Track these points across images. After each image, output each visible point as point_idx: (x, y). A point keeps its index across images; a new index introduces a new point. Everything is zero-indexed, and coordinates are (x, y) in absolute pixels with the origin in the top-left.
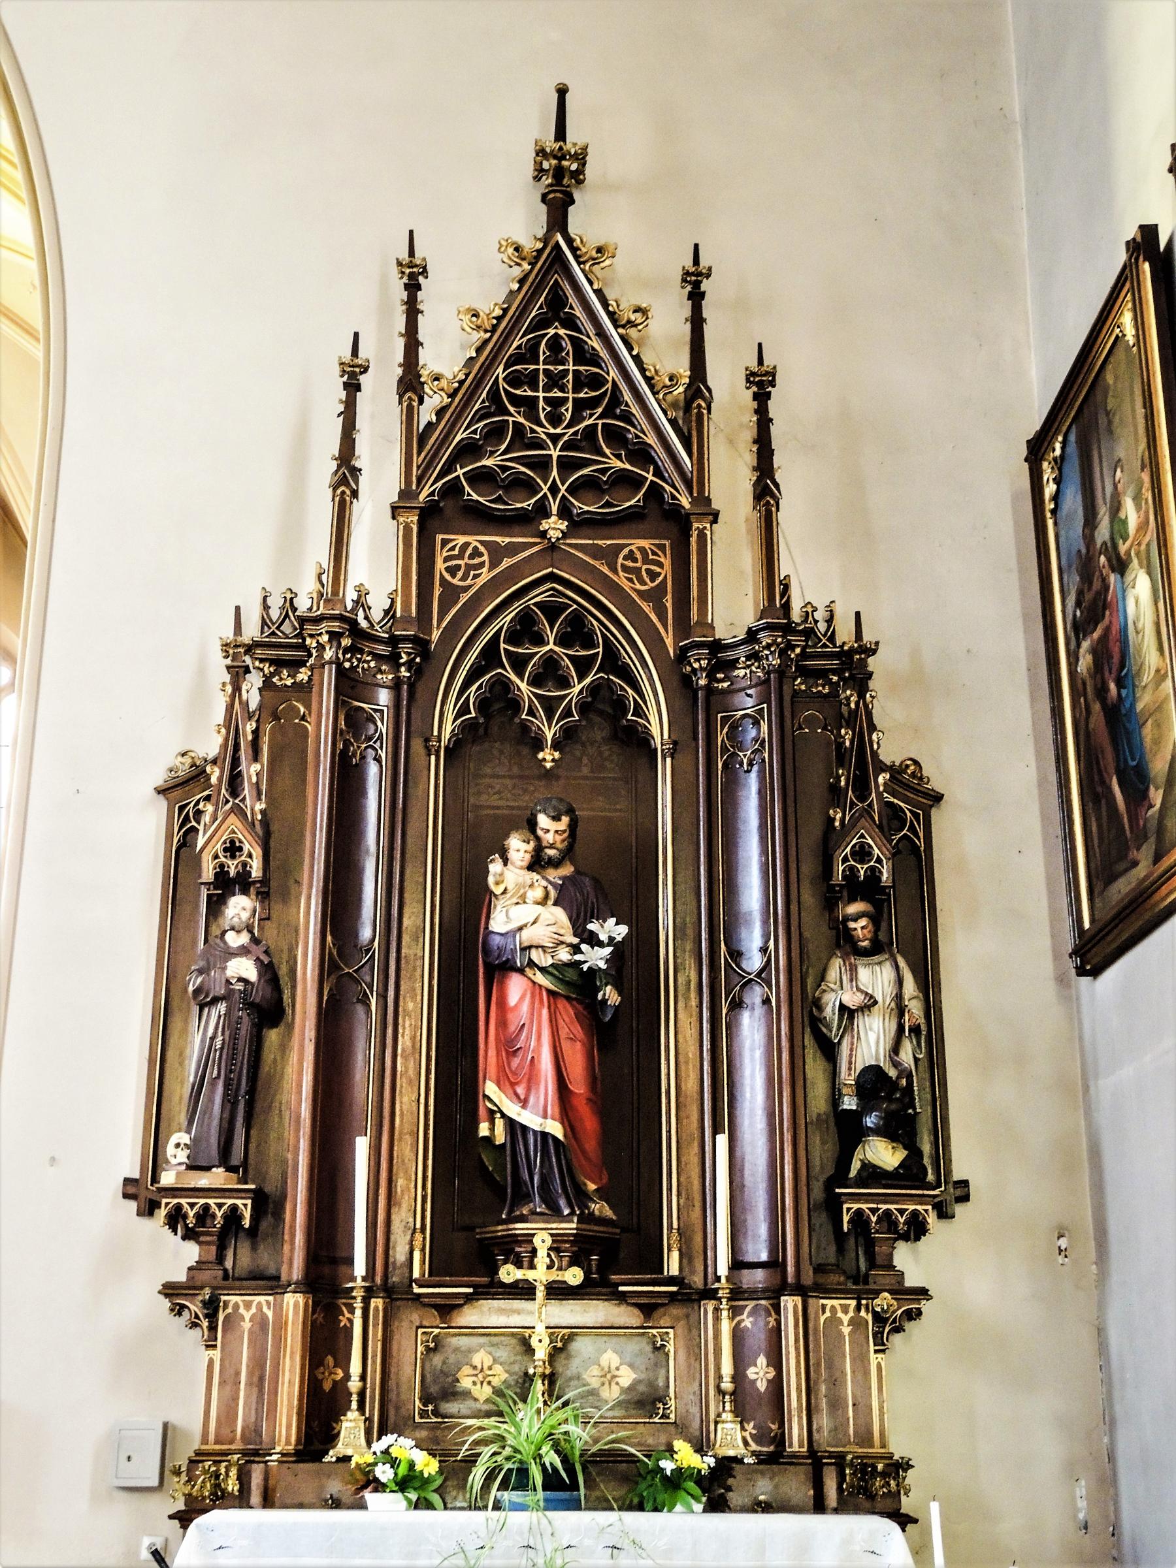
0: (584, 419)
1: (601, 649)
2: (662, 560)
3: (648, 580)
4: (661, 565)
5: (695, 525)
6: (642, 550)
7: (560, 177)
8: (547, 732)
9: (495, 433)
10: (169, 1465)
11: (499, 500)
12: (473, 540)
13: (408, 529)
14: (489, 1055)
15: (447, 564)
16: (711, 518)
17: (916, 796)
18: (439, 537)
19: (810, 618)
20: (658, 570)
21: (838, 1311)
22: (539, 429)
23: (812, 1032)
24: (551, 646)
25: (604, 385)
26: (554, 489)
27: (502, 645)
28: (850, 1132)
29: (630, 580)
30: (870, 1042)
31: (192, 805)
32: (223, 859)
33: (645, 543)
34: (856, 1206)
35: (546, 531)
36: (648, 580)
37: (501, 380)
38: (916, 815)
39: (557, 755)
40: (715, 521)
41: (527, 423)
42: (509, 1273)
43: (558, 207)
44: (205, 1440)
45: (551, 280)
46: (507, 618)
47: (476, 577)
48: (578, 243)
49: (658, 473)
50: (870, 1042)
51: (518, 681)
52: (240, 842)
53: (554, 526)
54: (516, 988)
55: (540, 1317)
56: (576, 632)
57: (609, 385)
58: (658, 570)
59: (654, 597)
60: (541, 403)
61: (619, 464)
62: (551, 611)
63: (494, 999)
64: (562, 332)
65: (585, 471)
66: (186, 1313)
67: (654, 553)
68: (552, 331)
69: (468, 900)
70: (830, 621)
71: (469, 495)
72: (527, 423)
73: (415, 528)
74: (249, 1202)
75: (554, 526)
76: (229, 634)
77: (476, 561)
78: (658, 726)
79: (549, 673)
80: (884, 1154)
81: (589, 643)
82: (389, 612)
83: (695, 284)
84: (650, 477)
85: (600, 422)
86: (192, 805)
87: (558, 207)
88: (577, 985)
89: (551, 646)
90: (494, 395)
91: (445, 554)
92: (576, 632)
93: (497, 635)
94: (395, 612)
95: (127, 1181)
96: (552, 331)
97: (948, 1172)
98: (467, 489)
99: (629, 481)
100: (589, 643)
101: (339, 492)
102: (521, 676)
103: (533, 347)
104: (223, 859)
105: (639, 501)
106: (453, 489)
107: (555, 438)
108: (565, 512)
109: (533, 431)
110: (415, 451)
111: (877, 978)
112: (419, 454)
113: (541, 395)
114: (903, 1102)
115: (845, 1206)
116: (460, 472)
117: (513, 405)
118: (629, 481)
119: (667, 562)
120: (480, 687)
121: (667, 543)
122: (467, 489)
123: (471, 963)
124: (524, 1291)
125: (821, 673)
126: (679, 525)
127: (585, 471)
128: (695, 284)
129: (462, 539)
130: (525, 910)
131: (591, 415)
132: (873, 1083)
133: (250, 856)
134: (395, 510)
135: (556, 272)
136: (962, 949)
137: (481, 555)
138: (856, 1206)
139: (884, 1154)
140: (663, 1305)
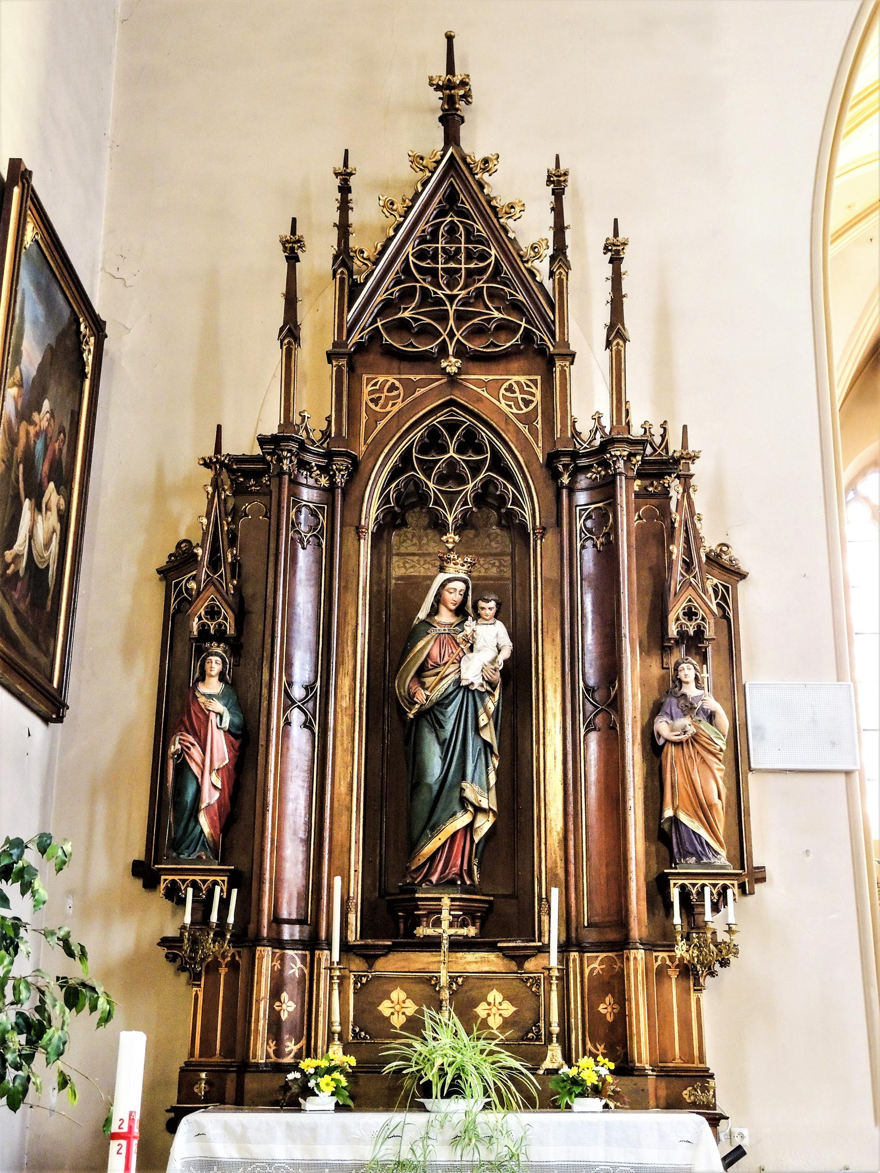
0: (474, 282)
1: (489, 455)
2: (534, 390)
3: (523, 407)
4: (533, 395)
5: (558, 364)
6: (518, 383)
8: (448, 516)
9: (407, 295)
11: (411, 345)
12: (391, 379)
13: (339, 368)
15: (371, 397)
16: (570, 358)
18: (365, 377)
19: (648, 434)
20: (530, 398)
22: (439, 292)
24: (451, 453)
25: (488, 259)
26: (451, 335)
27: (414, 454)
29: (510, 406)
31: (184, 582)
32: (205, 621)
33: (522, 379)
34: (170, 878)
35: (445, 368)
36: (523, 407)
37: (411, 258)
38: (727, 588)
39: (457, 538)
40: (572, 363)
41: (431, 288)
42: (423, 931)
43: (451, 121)
44: (192, 1054)
46: (417, 434)
47: (393, 405)
48: (469, 160)
49: (528, 322)
51: (428, 482)
52: (218, 607)
53: (452, 365)
55: (444, 966)
56: (470, 443)
57: (493, 258)
58: (530, 398)
59: (527, 420)
60: (440, 272)
61: (501, 316)
62: (452, 427)
64: (456, 219)
65: (476, 321)
66: (179, 960)
67: (528, 386)
68: (449, 219)
70: (663, 436)
71: (386, 340)
72: (431, 288)
73: (345, 369)
74: (226, 879)
75: (452, 365)
76: (210, 452)
77: (395, 393)
81: (480, 450)
82: (326, 434)
83: (557, 183)
84: (523, 324)
85: (485, 285)
86: (184, 582)
87: (451, 121)
89: (451, 453)
90: (406, 270)
91: (369, 388)
93: (410, 448)
94: (330, 433)
95: (763, 880)
96: (449, 219)
98: (385, 336)
99: (506, 328)
100: (480, 450)
101: (286, 341)
102: (429, 477)
103: (434, 234)
104: (205, 621)
105: (517, 341)
106: (375, 335)
107: (451, 298)
108: (461, 352)
109: (435, 293)
110: (346, 305)
112: (349, 311)
113: (440, 266)
115: (163, 877)
116: (379, 324)
117: (419, 273)
118: (506, 328)
119: (538, 393)
120: (397, 485)
121: (539, 378)
122: (385, 336)
124: (432, 944)
126: (546, 357)
127: (476, 321)
128: (557, 183)
129: (381, 379)
131: (479, 280)
133: (225, 619)
134: (330, 356)
135: (452, 176)
137: (397, 389)
138: (170, 878)
140: (533, 956)
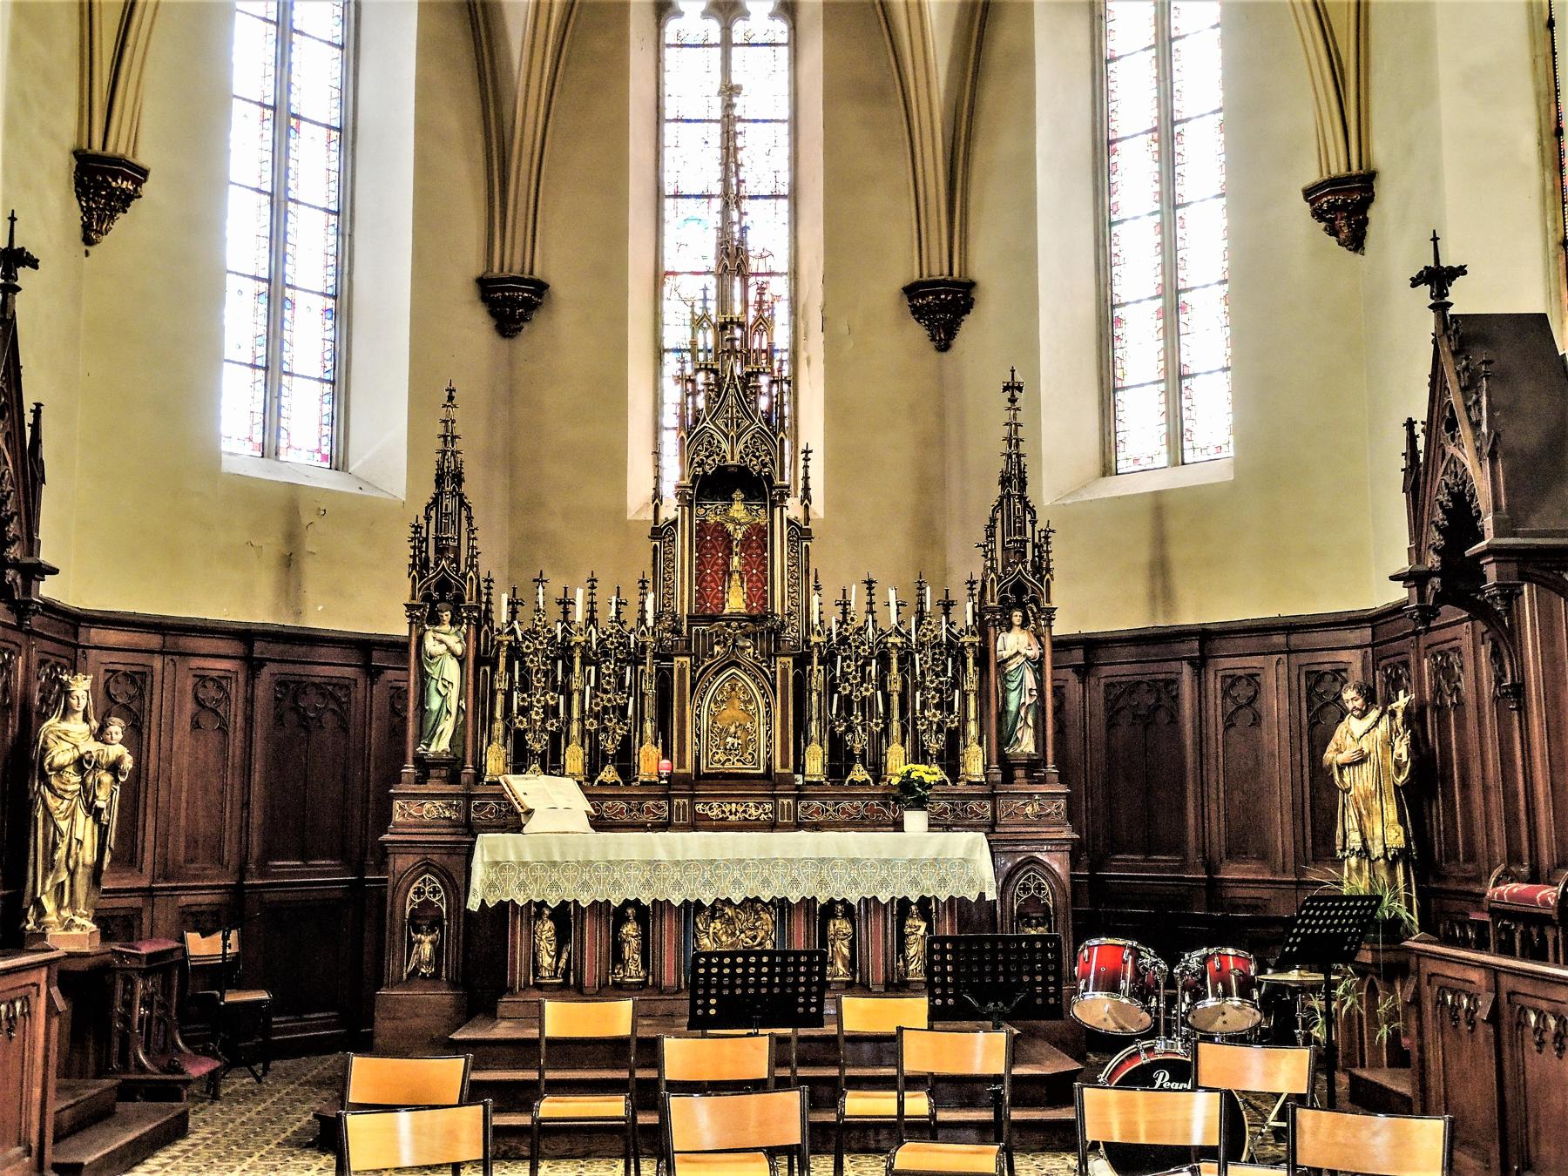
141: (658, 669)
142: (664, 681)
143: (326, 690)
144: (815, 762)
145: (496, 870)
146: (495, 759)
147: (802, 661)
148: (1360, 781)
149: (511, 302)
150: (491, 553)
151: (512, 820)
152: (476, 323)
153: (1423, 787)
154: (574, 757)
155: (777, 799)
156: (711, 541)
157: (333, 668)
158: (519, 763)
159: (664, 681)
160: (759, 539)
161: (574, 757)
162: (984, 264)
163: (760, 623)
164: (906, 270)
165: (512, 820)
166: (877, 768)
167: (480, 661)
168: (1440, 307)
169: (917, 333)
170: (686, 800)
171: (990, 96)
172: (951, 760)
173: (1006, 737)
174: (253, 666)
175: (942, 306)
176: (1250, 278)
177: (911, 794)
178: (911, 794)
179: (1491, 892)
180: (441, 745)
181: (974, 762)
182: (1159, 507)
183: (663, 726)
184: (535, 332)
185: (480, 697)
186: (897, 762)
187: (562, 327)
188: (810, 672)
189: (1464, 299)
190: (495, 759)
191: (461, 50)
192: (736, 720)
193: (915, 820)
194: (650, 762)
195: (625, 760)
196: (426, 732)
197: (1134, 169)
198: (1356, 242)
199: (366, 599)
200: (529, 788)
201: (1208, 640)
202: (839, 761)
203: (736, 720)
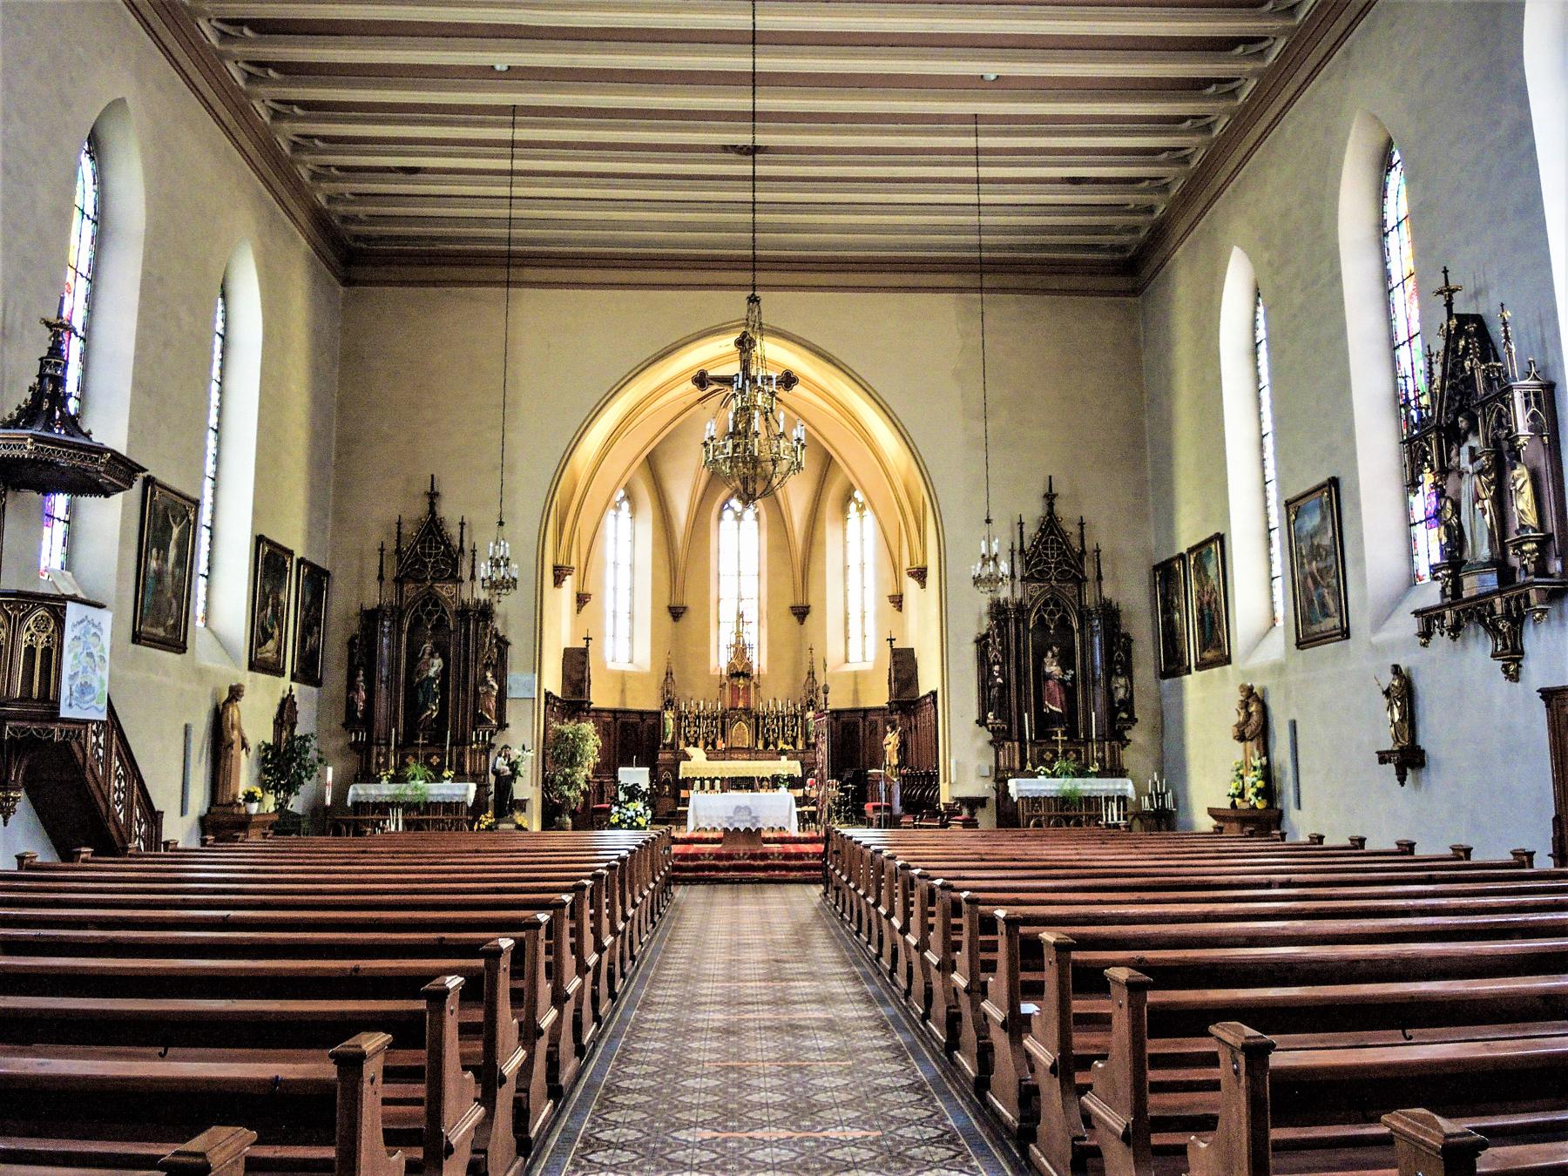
7: (1050, 497)
10: (1300, 503)
14: (1046, 693)
17: (1129, 640)
21: (1115, 743)
23: (1110, 693)
28: (1118, 711)
30: (1121, 693)
45: (1050, 523)
50: (1121, 693)
54: (1051, 683)
63: (1107, 220)
69: (1039, 664)
78: (1075, 626)
79: (1051, 613)
80: (1124, 715)
88: (1062, 682)
92: (1057, 604)
97: (159, 835)
111: (1122, 681)
114: (1128, 704)
123: (1042, 677)
125: (1110, 614)
126: (1080, 582)
130: (1052, 668)
132: (1121, 702)
136: (1138, 673)
139: (1124, 715)
141: (723, 721)
142: (723, 724)
143: (632, 725)
144: (760, 746)
145: (685, 769)
146: (682, 743)
147: (757, 719)
148: (889, 748)
149: (676, 613)
150: (677, 692)
151: (687, 758)
152: (668, 617)
153: (903, 748)
154: (701, 743)
155: (751, 753)
156: (734, 689)
157: (635, 719)
158: (688, 745)
159: (723, 724)
160: (747, 688)
161: (701, 743)
162: (812, 601)
163: (747, 711)
164: (791, 602)
165: (687, 758)
166: (776, 746)
167: (679, 718)
168: (1449, 305)
169: (794, 619)
170: (730, 753)
171: (815, 550)
172: (794, 744)
173: (808, 738)
174: (616, 719)
175: (801, 613)
176: (879, 616)
177: (783, 752)
178: (783, 752)
179: (431, 673)
180: (669, 740)
181: (800, 746)
182: (856, 675)
183: (723, 735)
184: (683, 620)
185: (678, 727)
186: (781, 745)
187: (691, 618)
188: (757, 721)
189: (896, 645)
190: (682, 743)
191: (664, 549)
192: (741, 733)
193: (784, 758)
194: (720, 745)
195: (714, 744)
196: (665, 737)
197: (854, 573)
198: (900, 609)
199: (646, 700)
200: (691, 750)
201: (866, 711)
202: (766, 745)
203: (741, 733)
